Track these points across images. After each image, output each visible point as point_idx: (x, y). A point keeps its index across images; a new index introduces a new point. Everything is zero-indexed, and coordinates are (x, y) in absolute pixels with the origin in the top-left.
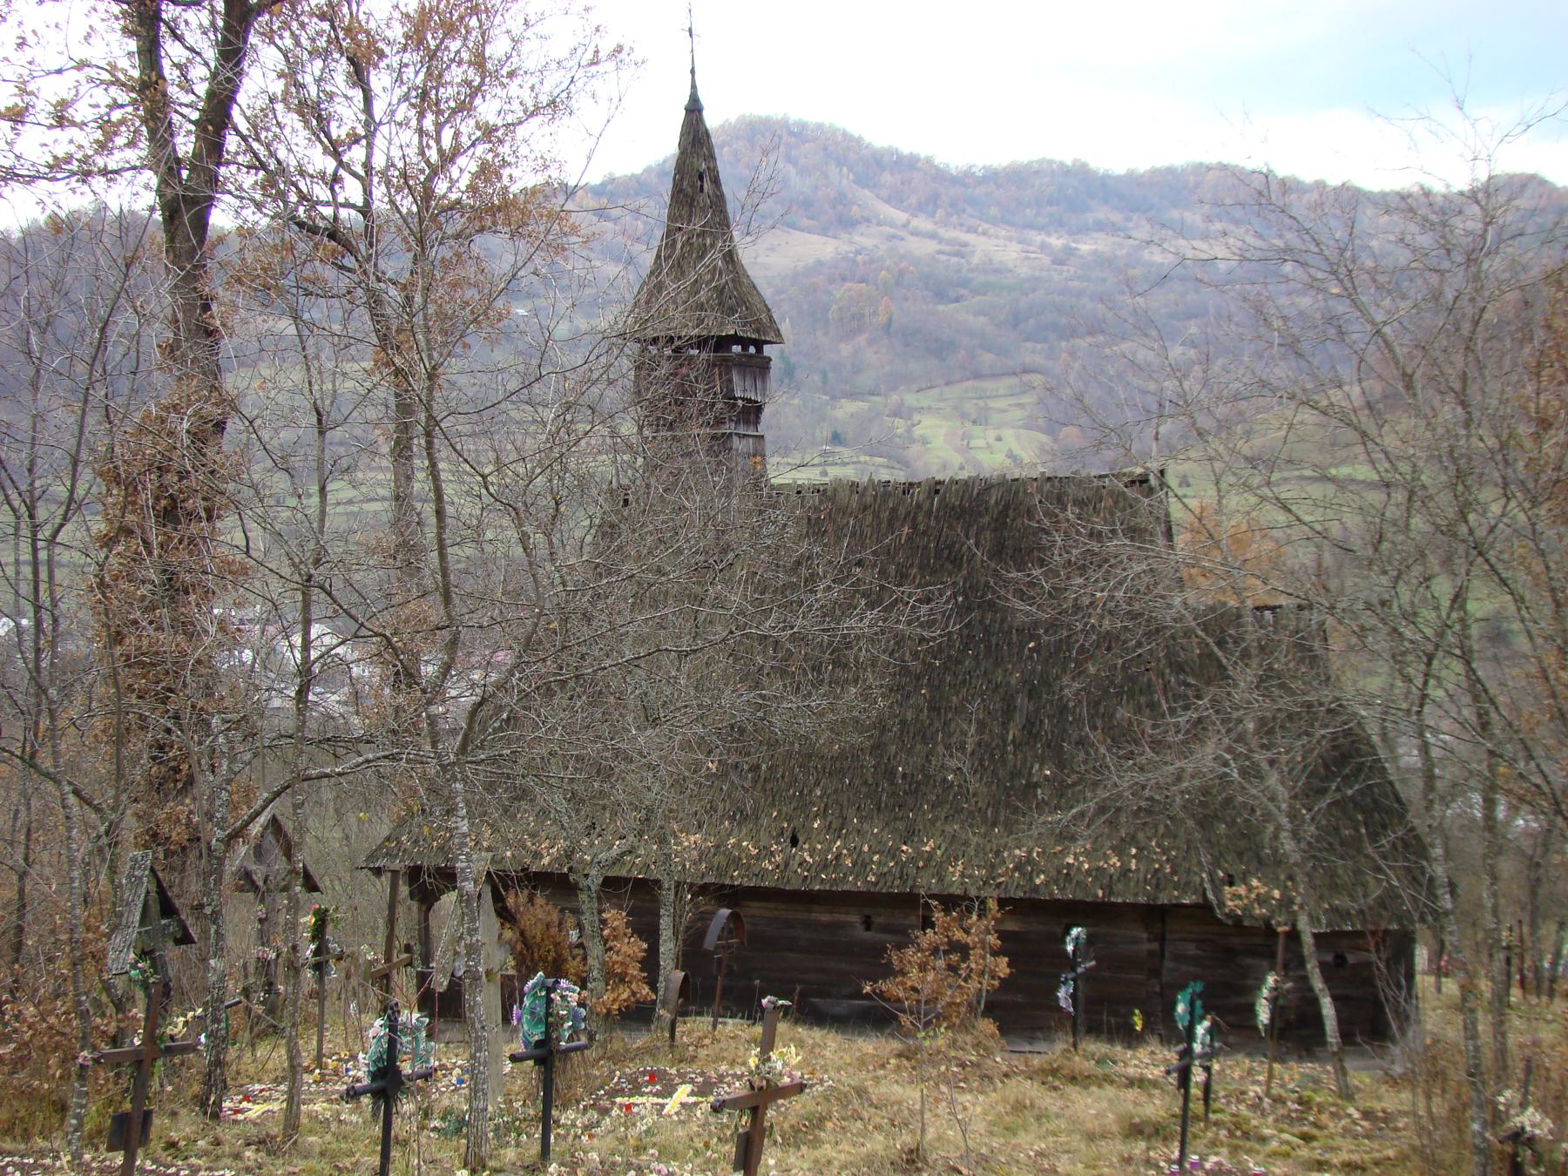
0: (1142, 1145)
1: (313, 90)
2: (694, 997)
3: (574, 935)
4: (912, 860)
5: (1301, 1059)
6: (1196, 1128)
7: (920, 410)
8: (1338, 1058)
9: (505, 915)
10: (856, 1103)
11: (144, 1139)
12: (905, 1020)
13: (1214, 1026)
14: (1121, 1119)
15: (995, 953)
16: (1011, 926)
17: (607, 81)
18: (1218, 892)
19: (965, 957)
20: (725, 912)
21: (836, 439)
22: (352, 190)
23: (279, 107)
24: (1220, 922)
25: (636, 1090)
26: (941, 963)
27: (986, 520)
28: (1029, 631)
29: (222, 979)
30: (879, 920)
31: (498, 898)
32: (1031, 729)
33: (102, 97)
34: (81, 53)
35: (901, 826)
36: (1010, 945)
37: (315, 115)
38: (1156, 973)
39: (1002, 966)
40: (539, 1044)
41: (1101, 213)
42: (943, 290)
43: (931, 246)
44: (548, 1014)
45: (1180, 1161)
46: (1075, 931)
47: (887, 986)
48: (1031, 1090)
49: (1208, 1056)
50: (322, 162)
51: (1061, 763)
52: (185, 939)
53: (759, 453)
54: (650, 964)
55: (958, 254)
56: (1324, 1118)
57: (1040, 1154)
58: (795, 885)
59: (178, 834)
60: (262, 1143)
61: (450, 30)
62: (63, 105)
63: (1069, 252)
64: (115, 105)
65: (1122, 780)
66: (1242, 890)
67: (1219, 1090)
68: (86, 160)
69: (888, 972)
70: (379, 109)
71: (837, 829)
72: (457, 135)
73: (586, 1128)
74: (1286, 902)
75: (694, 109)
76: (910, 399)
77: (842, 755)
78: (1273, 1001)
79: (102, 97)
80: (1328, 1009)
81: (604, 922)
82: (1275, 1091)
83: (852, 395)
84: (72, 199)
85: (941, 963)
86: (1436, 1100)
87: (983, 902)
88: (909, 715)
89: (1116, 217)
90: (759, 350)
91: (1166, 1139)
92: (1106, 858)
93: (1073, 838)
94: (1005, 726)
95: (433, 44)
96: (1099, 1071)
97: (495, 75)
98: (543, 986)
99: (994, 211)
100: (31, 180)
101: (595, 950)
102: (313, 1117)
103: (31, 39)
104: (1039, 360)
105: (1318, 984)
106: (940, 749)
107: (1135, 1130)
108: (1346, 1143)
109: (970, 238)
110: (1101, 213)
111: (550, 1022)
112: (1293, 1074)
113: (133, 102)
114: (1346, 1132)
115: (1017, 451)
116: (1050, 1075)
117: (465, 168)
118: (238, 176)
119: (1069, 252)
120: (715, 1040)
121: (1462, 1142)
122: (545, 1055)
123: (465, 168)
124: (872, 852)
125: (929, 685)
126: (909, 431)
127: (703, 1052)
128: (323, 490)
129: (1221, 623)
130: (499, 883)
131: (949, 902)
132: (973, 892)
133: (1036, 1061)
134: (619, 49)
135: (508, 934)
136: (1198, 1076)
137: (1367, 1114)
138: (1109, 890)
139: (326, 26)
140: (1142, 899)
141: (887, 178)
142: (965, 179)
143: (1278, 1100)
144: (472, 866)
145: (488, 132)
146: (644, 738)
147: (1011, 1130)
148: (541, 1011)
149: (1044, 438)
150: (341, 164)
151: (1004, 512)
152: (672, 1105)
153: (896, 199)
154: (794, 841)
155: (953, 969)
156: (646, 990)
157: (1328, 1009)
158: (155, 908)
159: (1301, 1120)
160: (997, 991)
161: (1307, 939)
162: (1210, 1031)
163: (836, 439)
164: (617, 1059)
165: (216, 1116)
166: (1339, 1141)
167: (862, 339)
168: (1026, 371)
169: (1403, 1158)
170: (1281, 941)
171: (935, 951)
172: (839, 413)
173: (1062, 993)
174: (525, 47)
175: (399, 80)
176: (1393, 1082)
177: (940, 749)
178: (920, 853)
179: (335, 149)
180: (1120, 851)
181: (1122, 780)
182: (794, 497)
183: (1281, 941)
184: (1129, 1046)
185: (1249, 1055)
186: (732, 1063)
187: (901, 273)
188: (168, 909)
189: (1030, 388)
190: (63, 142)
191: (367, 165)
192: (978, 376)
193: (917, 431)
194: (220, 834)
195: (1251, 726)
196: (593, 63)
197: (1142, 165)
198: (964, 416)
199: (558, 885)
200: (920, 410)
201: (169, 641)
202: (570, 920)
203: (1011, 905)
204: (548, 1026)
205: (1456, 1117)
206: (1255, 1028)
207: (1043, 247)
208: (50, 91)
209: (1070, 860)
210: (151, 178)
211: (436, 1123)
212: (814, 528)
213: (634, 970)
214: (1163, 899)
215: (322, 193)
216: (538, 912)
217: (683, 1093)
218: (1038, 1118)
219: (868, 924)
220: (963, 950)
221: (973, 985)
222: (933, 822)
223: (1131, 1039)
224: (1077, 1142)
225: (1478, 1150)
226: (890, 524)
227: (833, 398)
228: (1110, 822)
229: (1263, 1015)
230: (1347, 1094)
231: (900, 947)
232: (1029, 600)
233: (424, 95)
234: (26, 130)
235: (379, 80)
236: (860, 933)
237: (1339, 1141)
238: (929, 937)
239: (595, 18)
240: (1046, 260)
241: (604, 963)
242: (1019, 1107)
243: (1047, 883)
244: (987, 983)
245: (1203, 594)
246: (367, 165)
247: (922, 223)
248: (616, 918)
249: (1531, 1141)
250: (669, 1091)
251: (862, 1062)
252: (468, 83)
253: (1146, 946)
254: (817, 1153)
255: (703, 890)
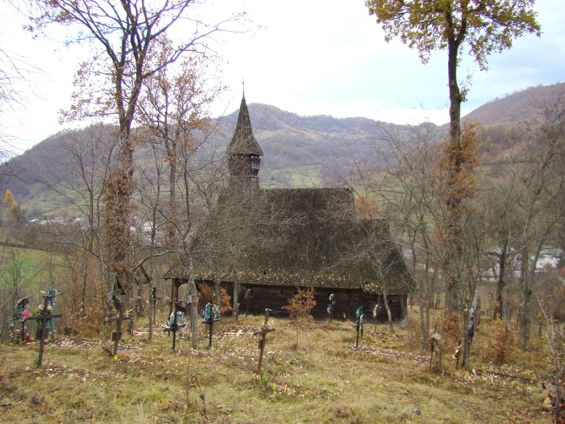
0: (348, 343)
1: (154, 95)
2: (242, 310)
3: (214, 294)
4: (293, 278)
5: (382, 324)
6: (359, 340)
7: (292, 172)
8: (391, 324)
9: (199, 290)
10: (281, 334)
11: (120, 339)
12: (291, 316)
13: (364, 316)
14: (342, 338)
15: (313, 300)
16: (316, 294)
17: (223, 94)
18: (364, 286)
19: (306, 301)
20: (249, 290)
21: (272, 179)
22: (162, 119)
23: (146, 99)
24: (363, 293)
25: (229, 331)
26: (300, 302)
27: (311, 198)
28: (322, 225)
29: (133, 303)
30: (284, 292)
31: (197, 286)
32: (321, 247)
33: (108, 97)
34: (103, 87)
35: (290, 270)
36: (316, 298)
37: (154, 101)
38: (348, 304)
39: (315, 303)
40: (209, 319)
41: (335, 128)
42: (298, 145)
43: (296, 134)
44: (211, 313)
45: (356, 347)
46: (331, 295)
47: (287, 308)
48: (321, 331)
49: (363, 323)
50: (155, 112)
51: (328, 255)
52: (123, 293)
53: (257, 182)
54: (232, 301)
55: (302, 136)
56: (388, 337)
57: (324, 346)
58: (265, 284)
59: (121, 269)
60: (144, 341)
61: (186, 82)
62: (99, 99)
63: (328, 136)
64: (110, 99)
65: (343, 260)
66: (369, 285)
67: (364, 331)
68: (103, 112)
69: (287, 304)
70: (169, 100)
71: (275, 271)
72: (187, 106)
73: (219, 339)
74: (379, 288)
75: (244, 101)
76: (290, 170)
77: (276, 254)
78: (377, 311)
79: (108, 97)
80: (389, 312)
81: (221, 292)
82: (377, 331)
83: (276, 169)
84: (96, 120)
85: (300, 302)
86: (414, 332)
87: (310, 288)
88: (292, 244)
89: (339, 129)
90: (258, 157)
91: (353, 342)
92: (338, 278)
93: (331, 273)
94: (315, 247)
95: (182, 85)
96: (336, 327)
97: (197, 92)
98: (210, 306)
99: (310, 126)
100: (91, 116)
101: (219, 298)
102: (155, 335)
103: (93, 84)
104: (321, 161)
105: (387, 307)
106: (299, 252)
107: (345, 340)
108: (393, 343)
109: (304, 132)
110: (335, 128)
111: (212, 314)
112: (380, 327)
113: (115, 98)
114: (393, 340)
115: (315, 183)
116: (325, 328)
117: (188, 114)
118: (136, 115)
119: (328, 136)
120: (247, 320)
121: (419, 342)
122: (210, 322)
123: (188, 114)
124: (283, 276)
125: (297, 237)
126: (290, 177)
127: (244, 322)
128: (159, 188)
129: (367, 224)
130: (199, 282)
131: (302, 288)
132: (307, 286)
133: (322, 325)
134: (226, 87)
135: (199, 294)
136: (361, 328)
137: (397, 336)
138: (339, 285)
139: (158, 81)
140: (346, 288)
141: (285, 118)
142: (304, 119)
143: (378, 333)
144: (193, 278)
145: (194, 105)
146: (231, 249)
147: (317, 340)
148: (209, 312)
149: (322, 180)
150: (160, 112)
151: (315, 197)
152: (238, 334)
153: (287, 123)
154: (265, 274)
155: (303, 303)
156: (231, 308)
157: (389, 312)
158: (117, 286)
159: (382, 338)
160: (313, 309)
161: (385, 297)
162: (363, 318)
163: (272, 179)
164: (224, 323)
165: (132, 335)
166: (391, 342)
167: (279, 155)
168: (317, 164)
169: (406, 345)
170: (379, 297)
171: (299, 299)
172: (273, 173)
173: (328, 309)
174: (204, 86)
175: (174, 94)
176: (402, 329)
177: (299, 252)
178: (294, 277)
179: (158, 109)
180: (341, 276)
181: (343, 260)
182: (265, 192)
183: (379, 297)
184: (342, 321)
185: (370, 323)
186: (251, 325)
187: (289, 140)
188: (120, 286)
189: (317, 168)
190: (99, 107)
191: (166, 113)
192: (306, 165)
193: (292, 177)
194: (132, 269)
195: (373, 247)
196: (219, 90)
197: (345, 117)
198: (303, 174)
199: (211, 283)
200: (292, 172)
201: (121, 224)
202: (214, 291)
203: (318, 289)
204: (211, 315)
205: (418, 337)
206: (373, 317)
207: (322, 135)
208: (96, 95)
209: (329, 278)
210: (117, 116)
211: (183, 337)
212: (272, 199)
213: (228, 303)
214: (351, 288)
215: (155, 119)
216: (206, 289)
217: (240, 332)
218: (323, 338)
219: (282, 293)
220: (305, 299)
221: (307, 307)
222: (298, 269)
223: (344, 320)
224: (332, 343)
225: (423, 343)
226: (288, 199)
227: (272, 169)
228: (339, 270)
229: (375, 314)
230: (393, 331)
231: (291, 298)
232: (322, 217)
233: (180, 97)
234: (90, 104)
235: (170, 93)
236: (280, 295)
237: (391, 342)
238: (297, 296)
239: (220, 80)
240: (322, 138)
241: (221, 301)
242: (319, 335)
243: (324, 284)
244: (311, 307)
245: (359, 218)
246: (166, 113)
247: (294, 129)
248: (224, 291)
249: (436, 341)
250: (237, 331)
251: (281, 325)
252: (190, 94)
253: (347, 299)
254: (272, 346)
255: (244, 284)
